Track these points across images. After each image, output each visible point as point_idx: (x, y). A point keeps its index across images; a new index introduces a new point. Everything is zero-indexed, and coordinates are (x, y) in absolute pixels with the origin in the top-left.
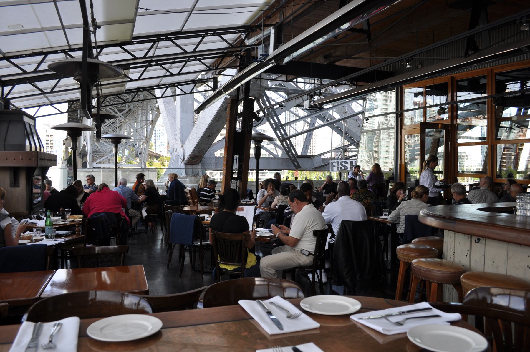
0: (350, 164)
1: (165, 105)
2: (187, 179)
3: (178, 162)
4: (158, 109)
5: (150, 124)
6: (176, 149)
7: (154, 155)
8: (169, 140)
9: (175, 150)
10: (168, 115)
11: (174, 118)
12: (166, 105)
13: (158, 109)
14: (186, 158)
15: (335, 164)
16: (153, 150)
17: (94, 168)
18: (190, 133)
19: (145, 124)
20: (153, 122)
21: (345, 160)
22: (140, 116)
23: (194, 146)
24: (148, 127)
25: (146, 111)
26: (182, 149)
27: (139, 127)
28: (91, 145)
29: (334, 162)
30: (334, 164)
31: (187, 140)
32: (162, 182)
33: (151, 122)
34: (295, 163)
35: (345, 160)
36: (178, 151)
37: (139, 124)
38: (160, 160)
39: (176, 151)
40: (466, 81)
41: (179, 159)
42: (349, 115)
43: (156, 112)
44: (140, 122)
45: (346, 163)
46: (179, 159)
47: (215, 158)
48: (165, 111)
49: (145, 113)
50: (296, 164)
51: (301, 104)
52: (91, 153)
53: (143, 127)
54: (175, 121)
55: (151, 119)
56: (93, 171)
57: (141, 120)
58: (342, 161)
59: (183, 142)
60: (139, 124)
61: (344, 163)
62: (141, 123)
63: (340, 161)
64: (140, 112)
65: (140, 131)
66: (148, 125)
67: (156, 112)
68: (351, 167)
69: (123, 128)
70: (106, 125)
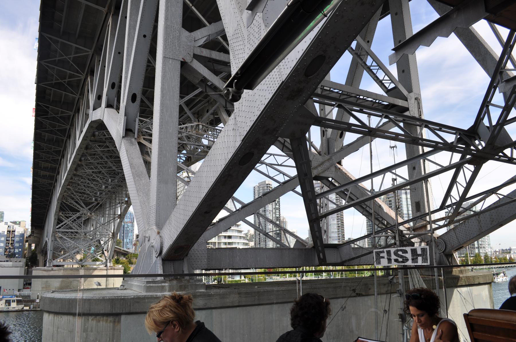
0: (412, 253)
1: (134, 178)
2: (166, 284)
3: (151, 257)
4: (127, 202)
5: (117, 218)
6: (149, 237)
7: (121, 252)
8: (148, 180)
9: (147, 239)
10: (137, 191)
11: (147, 195)
12: (137, 178)
13: (127, 202)
14: (165, 251)
15: (385, 255)
16: (121, 247)
17: (54, 266)
18: (171, 213)
19: (112, 218)
20: (122, 217)
21: (402, 248)
22: (108, 209)
23: (180, 230)
24: (116, 221)
25: (114, 204)
26: (158, 236)
27: (106, 221)
28: (52, 241)
29: (383, 252)
30: (382, 255)
31: (168, 222)
32: (125, 289)
33: (119, 216)
34: (321, 254)
35: (402, 248)
36: (152, 241)
37: (107, 218)
38: (128, 257)
39: (149, 241)
40: (503, 152)
41: (154, 251)
42: (417, 178)
43: (125, 205)
44: (107, 216)
45: (405, 252)
46: (154, 251)
47: (206, 251)
48: (134, 186)
49: (113, 206)
50: (321, 256)
51: (320, 175)
52: (52, 249)
53: (111, 222)
54: (149, 199)
55: (119, 213)
56: (52, 270)
57: (108, 214)
58: (396, 249)
59: (160, 225)
60: (107, 218)
61: (400, 253)
62: (108, 217)
63: (392, 250)
64: (108, 206)
65: (107, 225)
66: (116, 219)
67: (125, 205)
68: (415, 257)
69: (90, 224)
70: (71, 220)
